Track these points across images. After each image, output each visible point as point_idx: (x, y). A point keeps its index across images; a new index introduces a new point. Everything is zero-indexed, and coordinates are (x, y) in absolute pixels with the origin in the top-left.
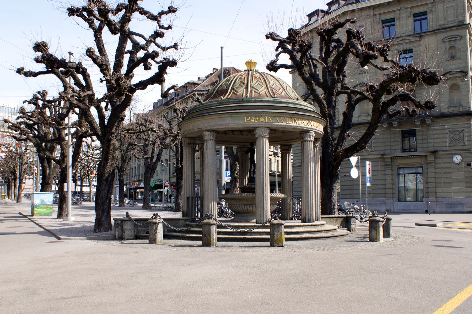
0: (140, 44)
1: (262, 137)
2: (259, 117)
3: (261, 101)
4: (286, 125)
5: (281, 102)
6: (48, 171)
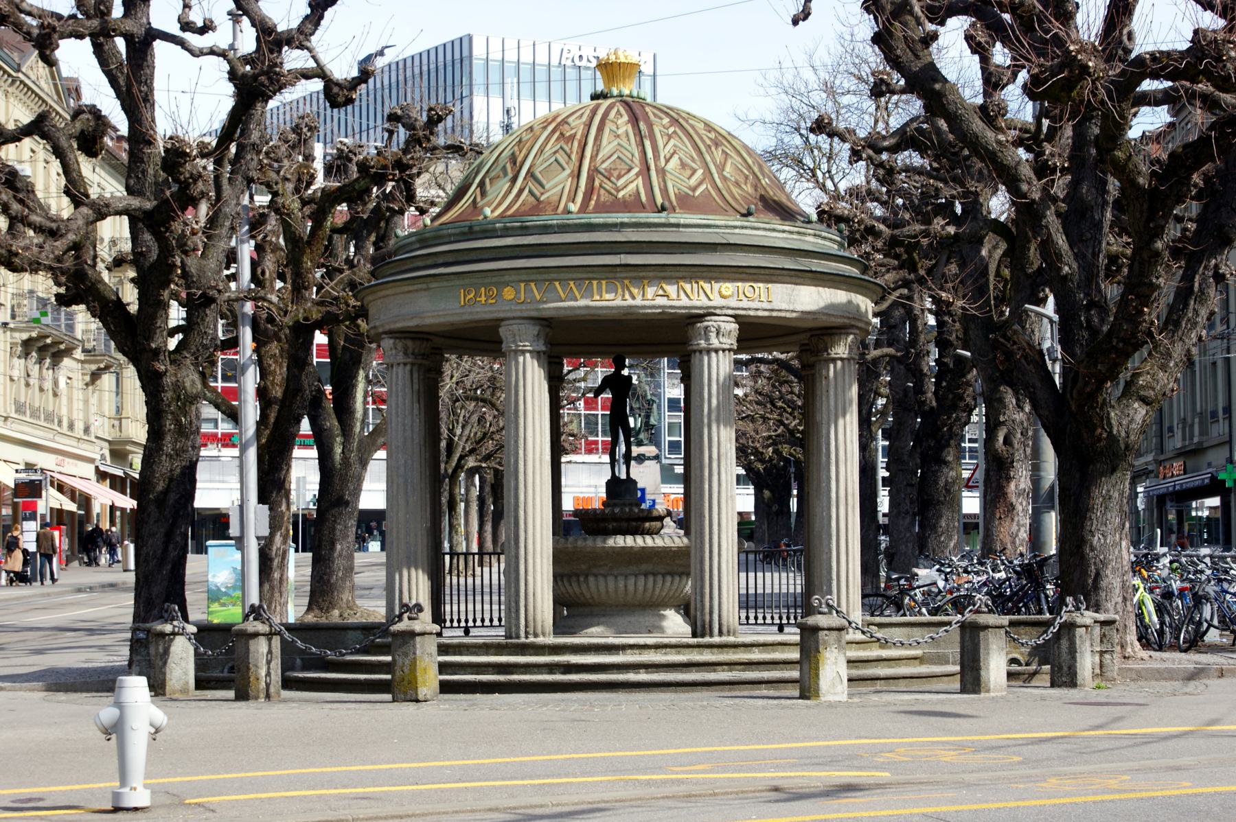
0: (279, 29)
1: (516, 352)
3: (522, 228)
4: (587, 307)
5: (590, 227)
6: (338, 450)
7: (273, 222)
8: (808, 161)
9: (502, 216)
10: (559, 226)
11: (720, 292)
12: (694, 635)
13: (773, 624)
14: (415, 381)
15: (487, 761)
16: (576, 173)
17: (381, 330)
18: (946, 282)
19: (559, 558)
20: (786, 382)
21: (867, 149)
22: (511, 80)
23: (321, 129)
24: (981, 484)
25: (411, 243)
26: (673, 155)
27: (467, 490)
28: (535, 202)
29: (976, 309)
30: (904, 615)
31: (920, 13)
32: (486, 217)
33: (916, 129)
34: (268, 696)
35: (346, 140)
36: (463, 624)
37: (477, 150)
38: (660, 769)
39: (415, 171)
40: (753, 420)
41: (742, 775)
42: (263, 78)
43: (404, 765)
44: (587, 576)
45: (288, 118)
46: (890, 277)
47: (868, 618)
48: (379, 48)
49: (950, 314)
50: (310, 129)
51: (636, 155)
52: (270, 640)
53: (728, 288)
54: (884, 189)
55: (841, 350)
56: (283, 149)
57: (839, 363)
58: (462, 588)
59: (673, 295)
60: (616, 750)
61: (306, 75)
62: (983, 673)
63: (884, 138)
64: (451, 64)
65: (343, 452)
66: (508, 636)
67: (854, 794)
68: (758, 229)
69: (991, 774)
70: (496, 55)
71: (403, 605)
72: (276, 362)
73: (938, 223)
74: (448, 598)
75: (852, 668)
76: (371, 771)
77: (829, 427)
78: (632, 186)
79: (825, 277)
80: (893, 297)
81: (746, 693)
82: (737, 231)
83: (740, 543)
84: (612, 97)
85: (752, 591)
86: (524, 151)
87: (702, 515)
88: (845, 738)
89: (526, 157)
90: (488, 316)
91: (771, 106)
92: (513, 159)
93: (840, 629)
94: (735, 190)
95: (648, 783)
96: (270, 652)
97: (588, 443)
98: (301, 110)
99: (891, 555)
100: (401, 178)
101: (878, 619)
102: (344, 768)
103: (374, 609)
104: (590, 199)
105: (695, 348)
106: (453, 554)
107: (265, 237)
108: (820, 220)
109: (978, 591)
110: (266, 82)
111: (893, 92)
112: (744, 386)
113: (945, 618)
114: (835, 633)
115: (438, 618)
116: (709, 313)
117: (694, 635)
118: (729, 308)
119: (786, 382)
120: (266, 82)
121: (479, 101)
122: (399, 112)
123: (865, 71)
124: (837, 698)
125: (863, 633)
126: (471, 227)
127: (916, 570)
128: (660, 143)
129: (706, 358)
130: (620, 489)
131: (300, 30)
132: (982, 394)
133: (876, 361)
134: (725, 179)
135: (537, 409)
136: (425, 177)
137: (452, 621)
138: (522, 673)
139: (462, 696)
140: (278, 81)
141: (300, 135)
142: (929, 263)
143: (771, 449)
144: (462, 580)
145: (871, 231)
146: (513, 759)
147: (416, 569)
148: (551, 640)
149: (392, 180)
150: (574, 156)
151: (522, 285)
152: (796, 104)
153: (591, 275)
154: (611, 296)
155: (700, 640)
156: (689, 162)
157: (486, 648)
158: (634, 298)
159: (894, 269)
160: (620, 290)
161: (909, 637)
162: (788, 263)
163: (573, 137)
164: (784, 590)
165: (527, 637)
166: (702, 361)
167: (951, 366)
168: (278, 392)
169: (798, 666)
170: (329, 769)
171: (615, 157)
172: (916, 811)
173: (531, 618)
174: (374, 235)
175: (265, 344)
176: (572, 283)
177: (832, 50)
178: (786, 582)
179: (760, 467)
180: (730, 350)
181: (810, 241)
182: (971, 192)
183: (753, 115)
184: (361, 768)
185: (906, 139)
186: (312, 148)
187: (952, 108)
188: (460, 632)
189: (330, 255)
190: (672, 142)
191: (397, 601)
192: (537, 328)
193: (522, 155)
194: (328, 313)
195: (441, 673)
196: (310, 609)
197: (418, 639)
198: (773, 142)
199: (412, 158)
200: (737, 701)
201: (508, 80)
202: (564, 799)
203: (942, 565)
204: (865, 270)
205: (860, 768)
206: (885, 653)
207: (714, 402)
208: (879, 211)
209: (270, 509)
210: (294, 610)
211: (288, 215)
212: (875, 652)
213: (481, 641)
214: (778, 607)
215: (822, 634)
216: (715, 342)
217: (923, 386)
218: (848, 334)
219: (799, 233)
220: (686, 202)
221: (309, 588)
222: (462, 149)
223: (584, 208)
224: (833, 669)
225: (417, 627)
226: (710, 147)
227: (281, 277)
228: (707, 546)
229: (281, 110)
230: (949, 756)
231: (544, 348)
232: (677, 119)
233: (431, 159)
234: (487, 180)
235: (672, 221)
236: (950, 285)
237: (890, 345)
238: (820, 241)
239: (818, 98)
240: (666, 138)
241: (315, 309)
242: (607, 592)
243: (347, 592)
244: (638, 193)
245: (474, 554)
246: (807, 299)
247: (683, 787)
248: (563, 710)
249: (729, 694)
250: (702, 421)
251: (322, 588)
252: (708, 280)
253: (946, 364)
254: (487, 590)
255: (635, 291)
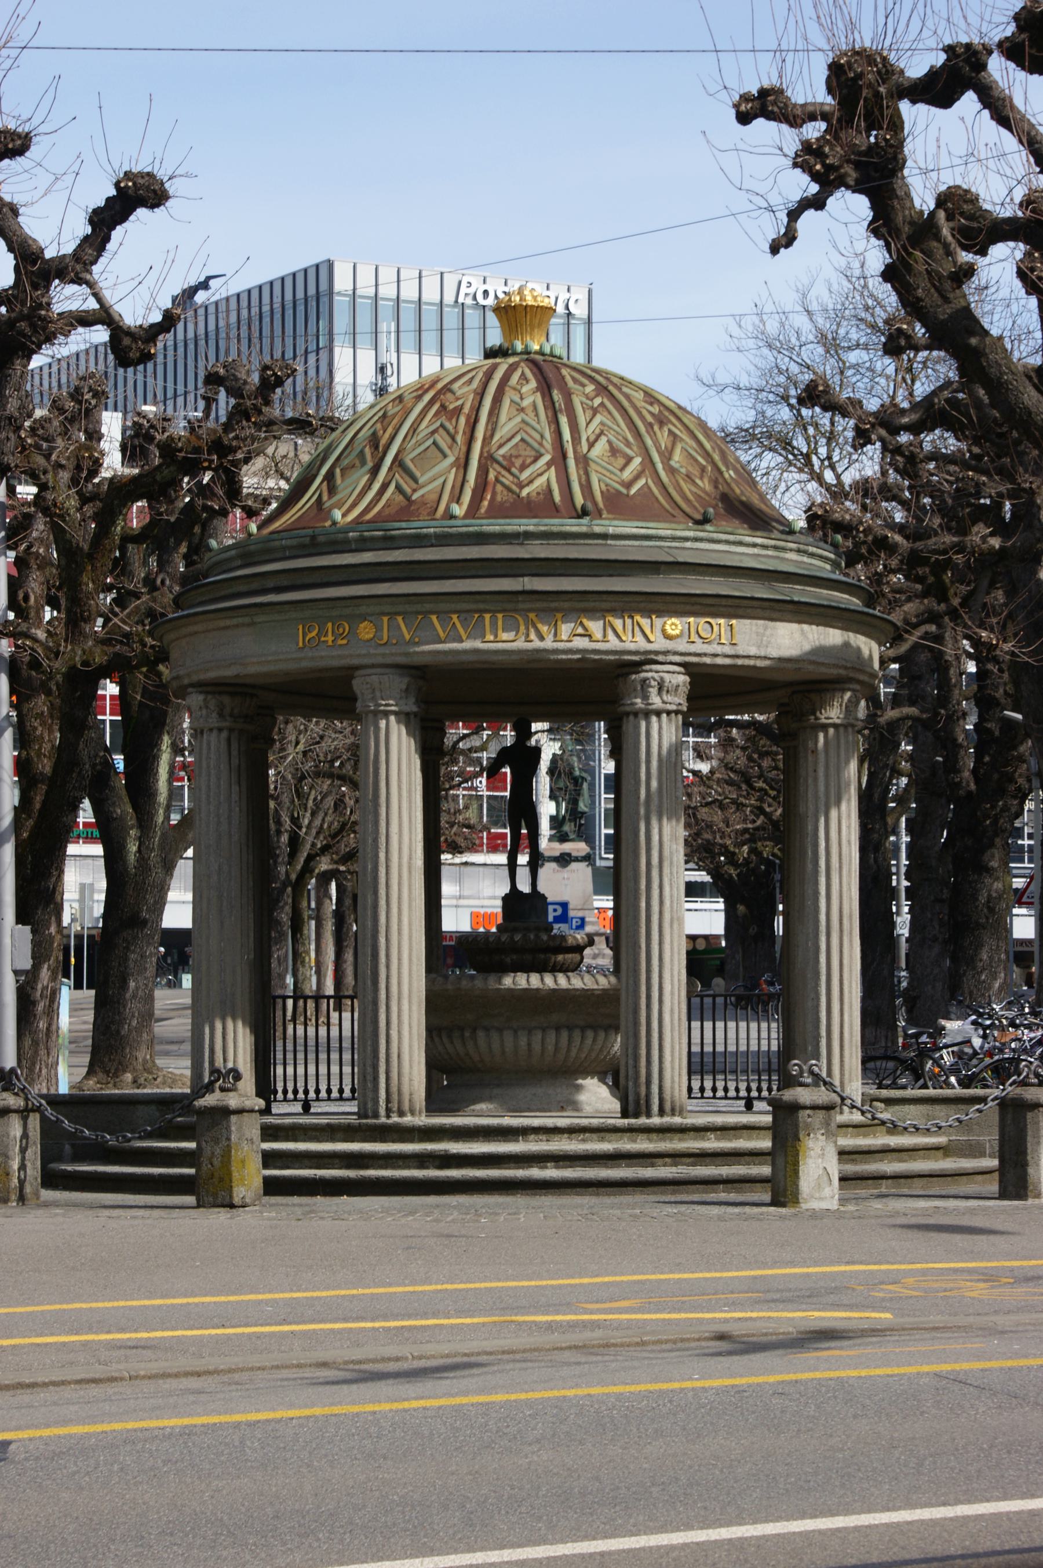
0: (48, 254)
2: (356, 619)
3: (385, 538)
4: (477, 651)
7: (40, 527)
8: (800, 443)
9: (357, 521)
10: (437, 536)
11: (664, 631)
12: (625, 1114)
13: (738, 1098)
14: (235, 753)
15: (324, 1294)
16: (462, 461)
17: (186, 681)
18: (988, 616)
19: (434, 1003)
20: (768, 753)
21: (877, 427)
22: (387, 325)
23: (111, 395)
24: (1036, 900)
25: (230, 559)
26: (598, 434)
27: (319, 904)
28: (405, 503)
29: (1030, 654)
30: (925, 1086)
31: (950, 238)
32: (334, 523)
33: (947, 400)
34: (22, 1198)
35: (145, 408)
36: (301, 1095)
37: (330, 424)
38: (566, 1307)
39: (240, 455)
40: (722, 807)
41: (683, 1315)
42: (23, 325)
43: (208, 1299)
44: (474, 1030)
45: (64, 380)
46: (911, 608)
47: (873, 1091)
48: (202, 279)
49: (996, 660)
50: (96, 395)
51: (547, 435)
52: (25, 1120)
53: (674, 625)
54: (907, 483)
55: (833, 713)
56: (56, 423)
57: (831, 731)
58: (311, 1042)
59: (598, 635)
60: (507, 1279)
61: (85, 320)
62: (1031, 1170)
63: (903, 412)
64: (304, 302)
65: (139, 851)
66: (362, 1114)
67: (832, 1344)
68: (719, 542)
69: (1035, 1316)
70: (366, 289)
71: (214, 1071)
72: (43, 724)
73: (981, 530)
74: (279, 1056)
75: (847, 1162)
76: (160, 1306)
77: (817, 821)
78: (542, 480)
79: (813, 610)
80: (913, 639)
81: (696, 1197)
82: (688, 544)
83: (690, 985)
84: (515, 354)
85: (708, 1049)
86: (390, 430)
87: (636, 945)
88: (832, 1263)
89: (392, 438)
90: (335, 663)
91: (746, 366)
92: (374, 440)
93: (829, 1108)
94: (685, 487)
95: (550, 1327)
96: (25, 1135)
97: (492, 837)
98: (82, 368)
99: (912, 1000)
100: (221, 465)
101: (885, 1093)
102: (122, 1303)
103: (175, 1072)
104: (482, 499)
105: (628, 709)
106: (298, 995)
107: (29, 547)
108: (811, 527)
109: (1030, 1052)
110: (28, 331)
111: (917, 349)
112: (709, 758)
113: (979, 1092)
114: (821, 1114)
115: (265, 1088)
116: (648, 659)
117: (625, 1114)
118: (676, 653)
119: (768, 753)
120: (28, 331)
121: (342, 356)
122: (222, 371)
123: (881, 315)
124: (824, 1205)
125: (863, 1113)
126: (313, 537)
127: (943, 1022)
128: (582, 420)
129: (643, 724)
130: (522, 907)
131: (77, 255)
132: (1038, 774)
133: (893, 726)
134: (672, 471)
135: (405, 794)
136: (259, 462)
137: (285, 1092)
138: (382, 1167)
139: (296, 1199)
140: (44, 329)
141: (80, 406)
142: (964, 589)
143: (745, 848)
144: (311, 1031)
145: (881, 544)
146: (361, 1291)
147: (234, 1020)
148: (422, 1120)
149: (209, 468)
150: (459, 438)
151: (385, 619)
152: (784, 363)
153: (482, 606)
154: (511, 635)
155: (633, 1121)
156: (622, 446)
157: (331, 1132)
158: (542, 638)
159: (916, 596)
160: (522, 628)
161: (929, 1117)
162: (760, 591)
163: (460, 409)
164: (754, 1047)
165: (388, 1117)
166: (637, 728)
167: (997, 733)
168: (45, 766)
169: (769, 1158)
170: (100, 1305)
171: (517, 438)
172: (926, 1368)
173: (394, 1089)
174: (184, 544)
175: (28, 698)
176: (455, 617)
177: (835, 287)
178: (759, 1035)
179: (733, 872)
180: (677, 712)
181: (792, 560)
182: (1024, 490)
183: (722, 378)
184: (147, 1302)
185: (931, 414)
186: (99, 422)
187: (993, 371)
188: (298, 1108)
189: (123, 572)
190: (598, 418)
191: (207, 1065)
192: (406, 680)
193: (387, 435)
194: (117, 655)
195: (266, 1165)
196: (91, 1072)
197: (234, 1118)
198: (751, 415)
199: (236, 438)
200: (683, 1208)
201: (383, 327)
202: (430, 1349)
203: (980, 1015)
204: (870, 600)
205: (851, 1307)
206: (894, 1141)
207: (654, 784)
208: (899, 517)
209: (33, 932)
210: (66, 1076)
211: (62, 517)
212: (881, 1140)
213: (323, 1121)
214: (746, 1072)
215: (803, 1114)
216: (656, 701)
217: (957, 761)
218: (844, 691)
219: (776, 548)
220: (617, 503)
221: (90, 1042)
222: (310, 424)
223: (473, 511)
224: (819, 1165)
225: (233, 1101)
226: (651, 425)
227: (54, 604)
228: (643, 988)
229: (55, 369)
230: (979, 1290)
231: (415, 709)
232: (607, 386)
233: (266, 438)
234: (338, 471)
235: (597, 530)
236: (994, 620)
237: (912, 703)
238: (805, 559)
239: (814, 353)
240: (589, 413)
241: (98, 650)
242: (503, 1052)
243: (144, 1047)
244: (549, 490)
245: (328, 998)
246: (787, 640)
247: (598, 1334)
248: (437, 1221)
249: (673, 1199)
250: (638, 813)
251: (108, 1045)
252: (648, 613)
253: (989, 731)
254: (334, 1044)
255: (544, 629)
